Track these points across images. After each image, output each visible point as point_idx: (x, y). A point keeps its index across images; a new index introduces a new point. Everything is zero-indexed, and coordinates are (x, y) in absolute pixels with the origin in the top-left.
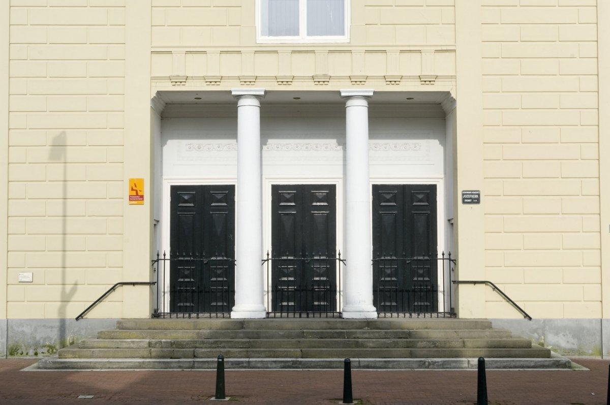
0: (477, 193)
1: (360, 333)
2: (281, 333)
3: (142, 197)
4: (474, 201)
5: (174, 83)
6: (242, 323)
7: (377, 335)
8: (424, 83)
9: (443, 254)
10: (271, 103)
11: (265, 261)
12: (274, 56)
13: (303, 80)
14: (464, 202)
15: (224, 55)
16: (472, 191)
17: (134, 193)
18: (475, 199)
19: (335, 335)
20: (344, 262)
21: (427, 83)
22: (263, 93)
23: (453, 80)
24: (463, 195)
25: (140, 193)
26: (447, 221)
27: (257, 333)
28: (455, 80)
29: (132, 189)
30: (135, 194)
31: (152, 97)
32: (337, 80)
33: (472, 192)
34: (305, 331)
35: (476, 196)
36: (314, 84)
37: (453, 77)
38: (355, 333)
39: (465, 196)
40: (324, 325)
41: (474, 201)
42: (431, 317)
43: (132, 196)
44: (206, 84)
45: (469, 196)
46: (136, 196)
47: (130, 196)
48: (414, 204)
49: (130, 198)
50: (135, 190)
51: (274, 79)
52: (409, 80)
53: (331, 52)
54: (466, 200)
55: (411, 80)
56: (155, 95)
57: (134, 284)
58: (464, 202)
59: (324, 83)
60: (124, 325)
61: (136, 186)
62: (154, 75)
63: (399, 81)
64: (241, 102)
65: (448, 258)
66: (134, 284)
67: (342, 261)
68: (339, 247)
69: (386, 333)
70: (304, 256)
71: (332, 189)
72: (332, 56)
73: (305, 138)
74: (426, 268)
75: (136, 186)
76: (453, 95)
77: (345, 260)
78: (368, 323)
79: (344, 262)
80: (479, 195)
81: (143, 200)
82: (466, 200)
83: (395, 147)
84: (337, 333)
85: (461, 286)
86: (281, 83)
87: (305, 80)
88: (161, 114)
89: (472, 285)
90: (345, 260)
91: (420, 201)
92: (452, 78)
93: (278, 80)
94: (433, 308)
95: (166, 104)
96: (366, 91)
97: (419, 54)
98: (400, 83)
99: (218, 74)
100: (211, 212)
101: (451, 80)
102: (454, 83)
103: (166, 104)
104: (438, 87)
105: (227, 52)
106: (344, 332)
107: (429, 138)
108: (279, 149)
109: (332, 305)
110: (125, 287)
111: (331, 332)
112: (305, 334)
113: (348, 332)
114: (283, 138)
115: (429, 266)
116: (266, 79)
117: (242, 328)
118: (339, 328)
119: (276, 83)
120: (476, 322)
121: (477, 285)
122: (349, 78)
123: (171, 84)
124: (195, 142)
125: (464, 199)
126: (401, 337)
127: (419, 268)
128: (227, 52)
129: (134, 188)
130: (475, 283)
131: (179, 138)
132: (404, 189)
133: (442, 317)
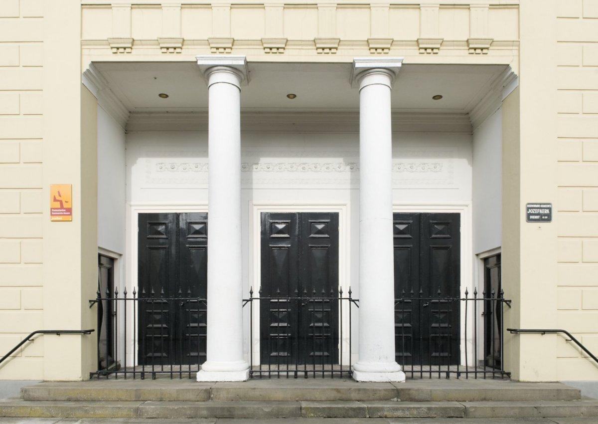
0: (548, 206)
1: (389, 409)
2: (266, 410)
3: (69, 210)
4: (543, 217)
5: (115, 50)
6: (209, 392)
7: (415, 412)
8: (472, 51)
9: (467, 293)
11: (248, 301)
12: (258, 12)
13: (300, 47)
14: (529, 220)
16: (541, 204)
17: (58, 205)
18: (545, 215)
19: (351, 413)
20: (357, 302)
21: (478, 51)
22: (242, 63)
23: (514, 48)
24: (528, 209)
25: (66, 206)
26: (475, 257)
27: (229, 410)
28: (517, 48)
29: (55, 200)
30: (59, 207)
31: (84, 70)
32: (349, 47)
33: (541, 206)
34: (304, 405)
35: (547, 211)
36: (315, 52)
37: (516, 44)
38: (382, 409)
39: (530, 211)
40: (333, 395)
41: (543, 217)
42: (476, 378)
43: (55, 209)
45: (537, 211)
46: (61, 209)
47: (51, 209)
48: (433, 236)
49: (51, 212)
50: (58, 201)
51: (259, 45)
52: (452, 48)
54: (531, 217)
56: (88, 67)
57: (58, 333)
58: (529, 220)
60: (31, 393)
61: (60, 196)
62: (87, 38)
64: (215, 78)
65: (474, 298)
66: (58, 333)
67: (353, 301)
68: (345, 282)
69: (429, 409)
70: (299, 294)
71: (333, 219)
73: (302, 156)
74: (406, 312)
75: (60, 196)
76: (514, 69)
77: (358, 300)
78: (397, 393)
79: (357, 302)
80: (550, 209)
81: (71, 214)
82: (531, 217)
84: (353, 409)
85: (523, 337)
86: (268, 50)
88: (126, 126)
89: (538, 336)
90: (358, 300)
92: (513, 46)
93: (265, 45)
94: (455, 359)
95: (130, 112)
97: (465, 12)
98: (440, 52)
99: (176, 35)
100: (187, 246)
101: (511, 48)
102: (515, 52)
103: (130, 112)
104: (492, 58)
106: (363, 409)
107: (452, 157)
108: (270, 169)
109: (333, 357)
110: (46, 336)
111: (344, 408)
112: (303, 411)
113: (371, 408)
115: (411, 310)
116: (248, 45)
117: (209, 398)
118: (354, 399)
119: (263, 52)
120: (558, 390)
121: (547, 336)
122: (366, 43)
123: (111, 51)
124: (168, 161)
125: (529, 215)
126: (452, 415)
127: (317, 311)
129: (58, 198)
130: (543, 332)
131: (148, 156)
133: (481, 378)
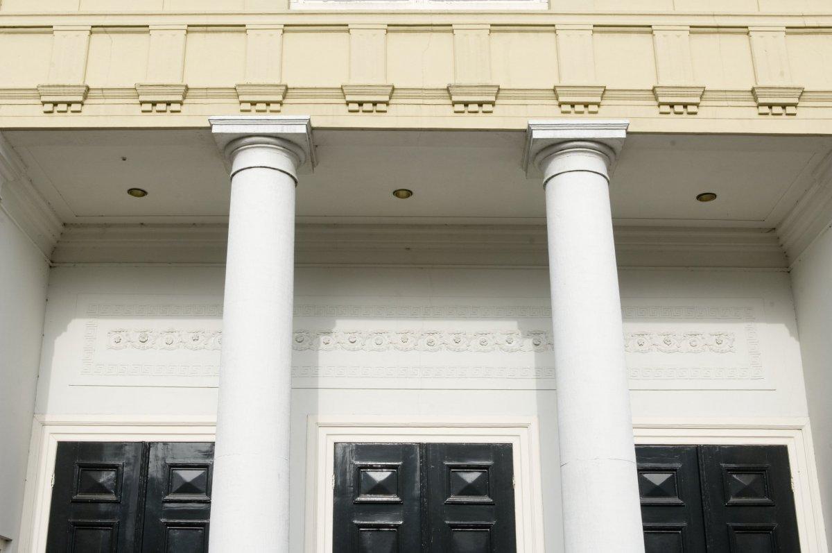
5: (49, 107)
8: (766, 110)
10: (335, 226)
15: (197, 39)
22: (302, 129)
44: (139, 108)
52: (725, 103)
53: (496, 28)
55: (730, 103)
59: (480, 110)
63: (697, 105)
72: (499, 39)
83: (667, 342)
86: (356, 107)
87: (426, 101)
88: (52, 253)
91: (745, 492)
95: (65, 224)
96: (607, 127)
97: (741, 40)
103: (65, 224)
105: (206, 28)
114: (366, 316)
124: (133, 326)
128: (206, 28)
132: (698, 451)
